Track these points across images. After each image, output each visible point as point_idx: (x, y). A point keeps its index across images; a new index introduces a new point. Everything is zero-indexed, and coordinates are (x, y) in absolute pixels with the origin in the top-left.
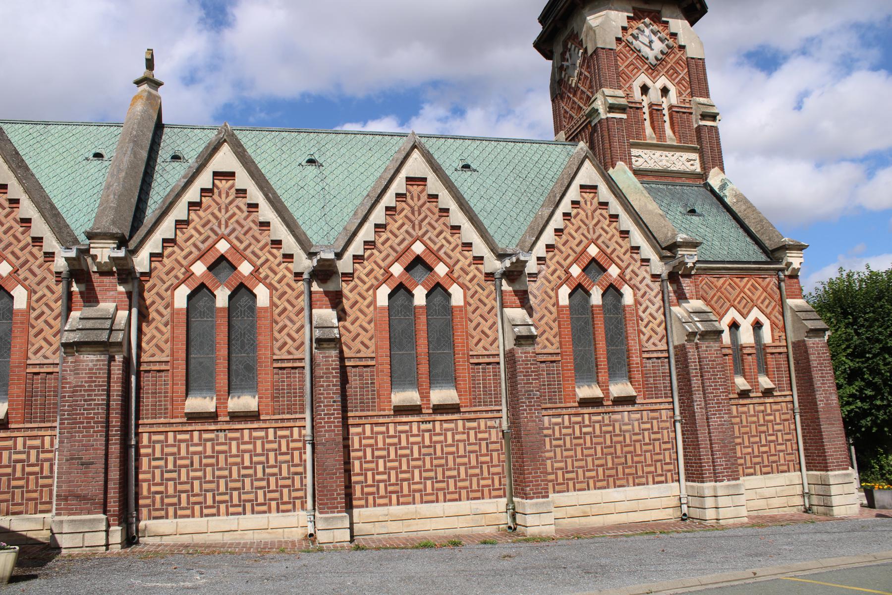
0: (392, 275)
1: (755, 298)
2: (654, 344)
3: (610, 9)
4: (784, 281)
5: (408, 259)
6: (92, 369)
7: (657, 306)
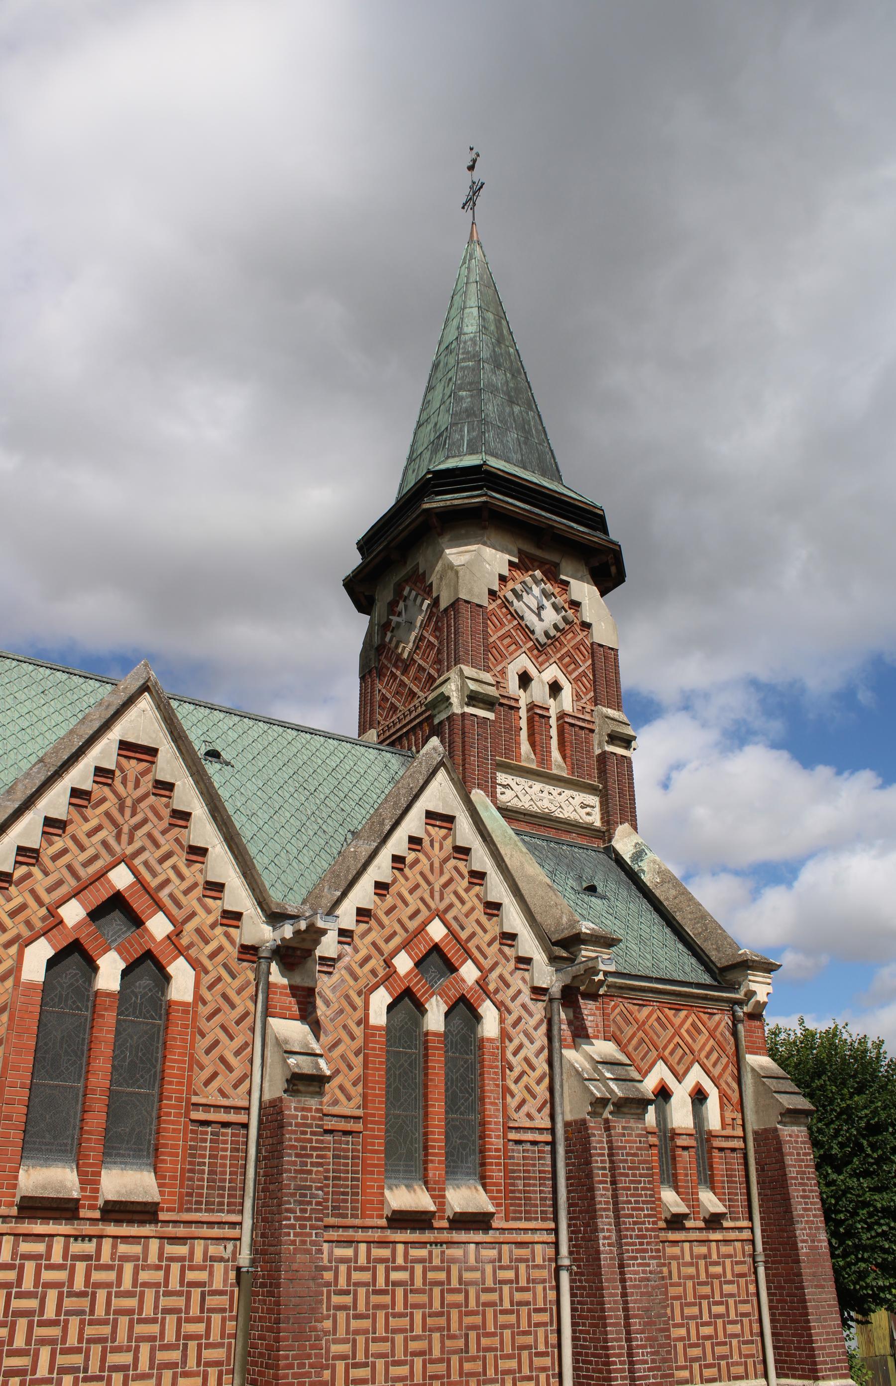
0: (62, 922)
1: (696, 1048)
2: (529, 1116)
3: (485, 544)
4: (742, 1021)
5: (101, 894)
7: (538, 1044)
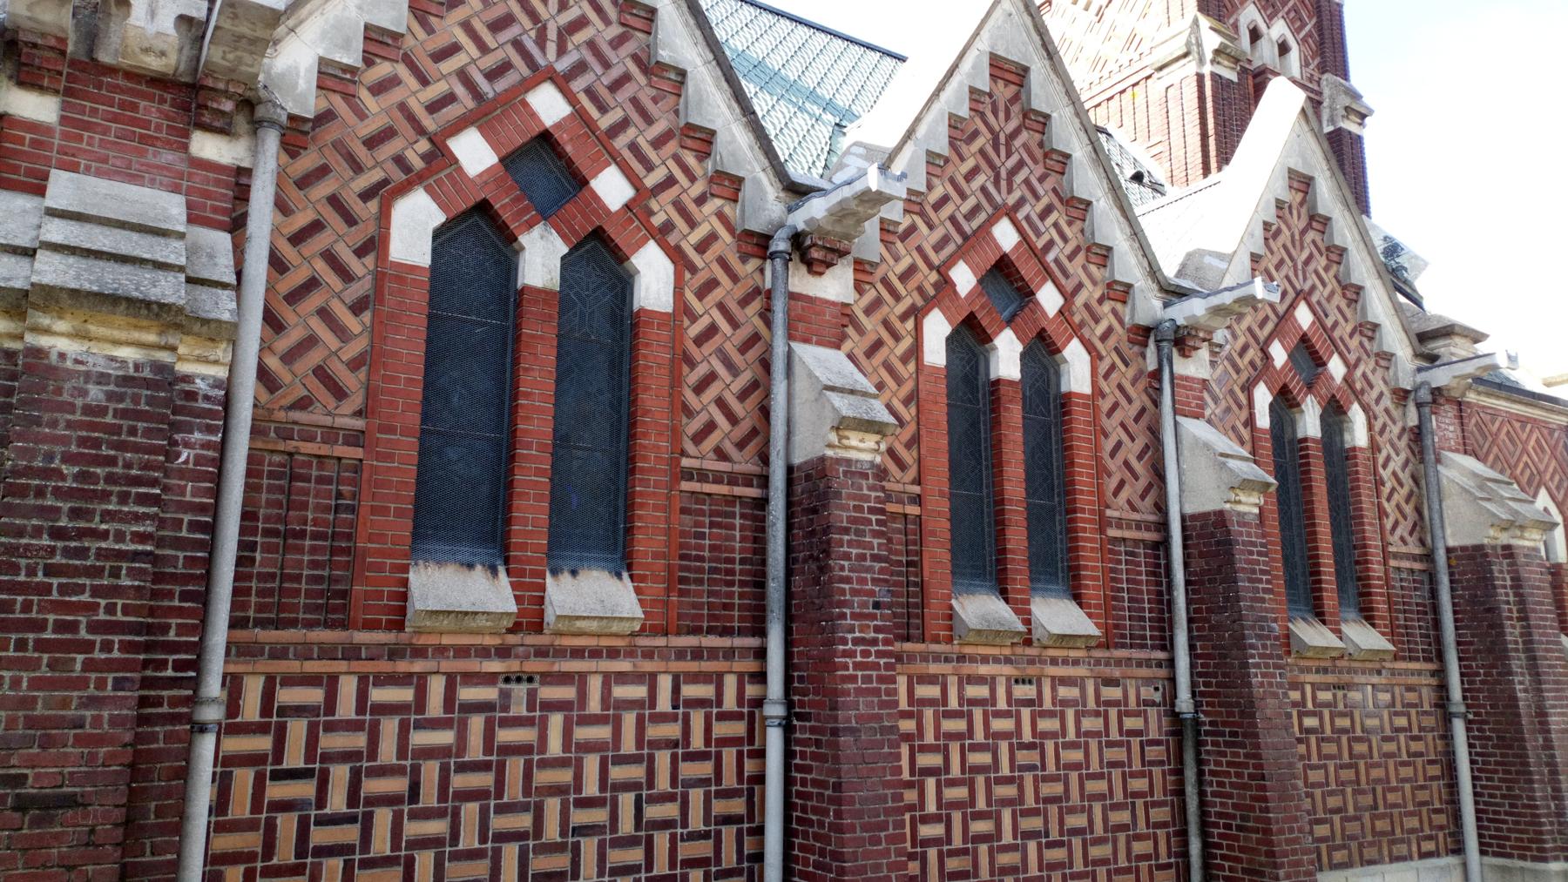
6: (102, 411)
